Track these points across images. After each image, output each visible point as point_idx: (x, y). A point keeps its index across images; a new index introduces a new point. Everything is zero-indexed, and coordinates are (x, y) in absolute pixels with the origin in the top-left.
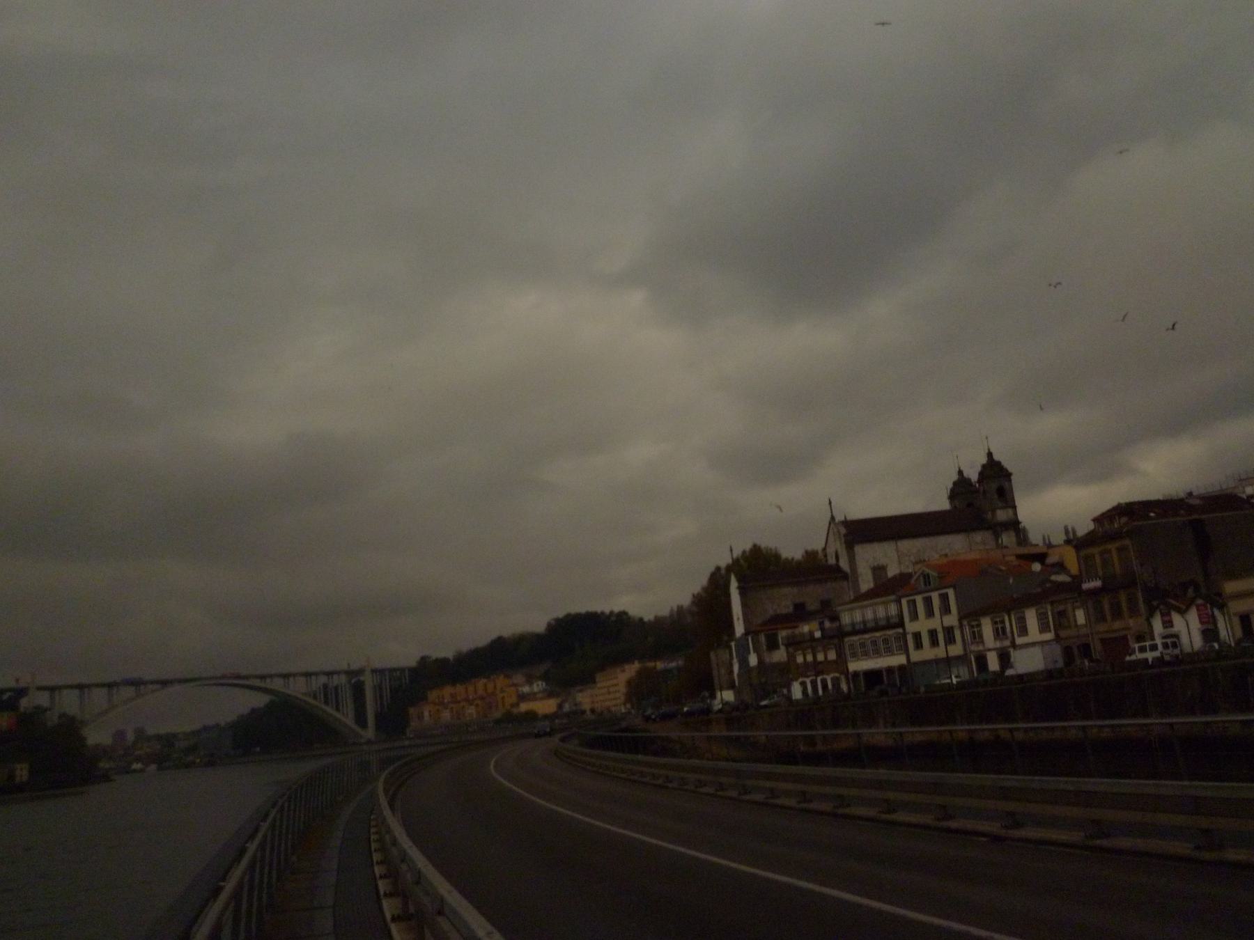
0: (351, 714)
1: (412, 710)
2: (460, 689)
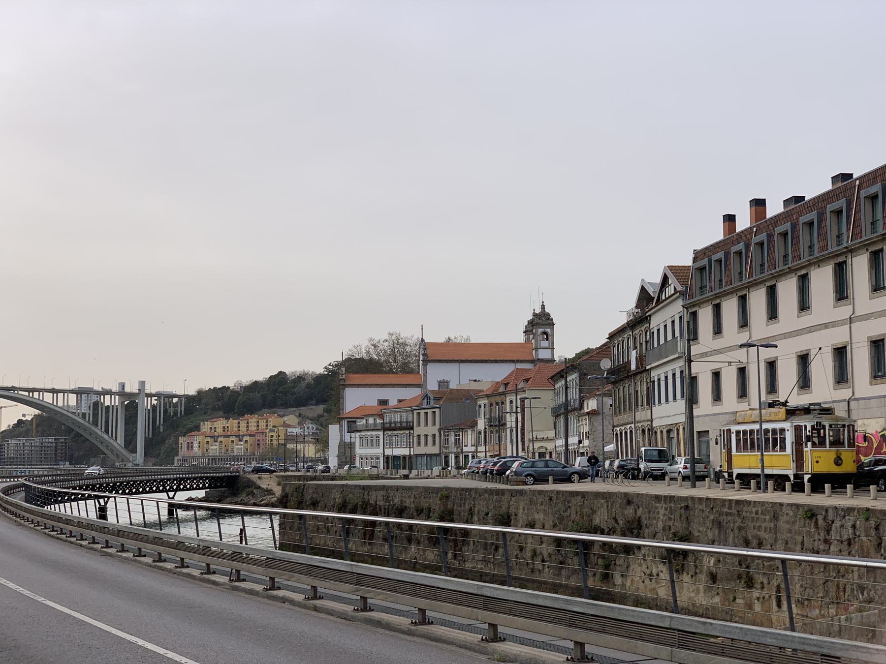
0: (121, 440)
1: (181, 440)
2: (232, 423)
